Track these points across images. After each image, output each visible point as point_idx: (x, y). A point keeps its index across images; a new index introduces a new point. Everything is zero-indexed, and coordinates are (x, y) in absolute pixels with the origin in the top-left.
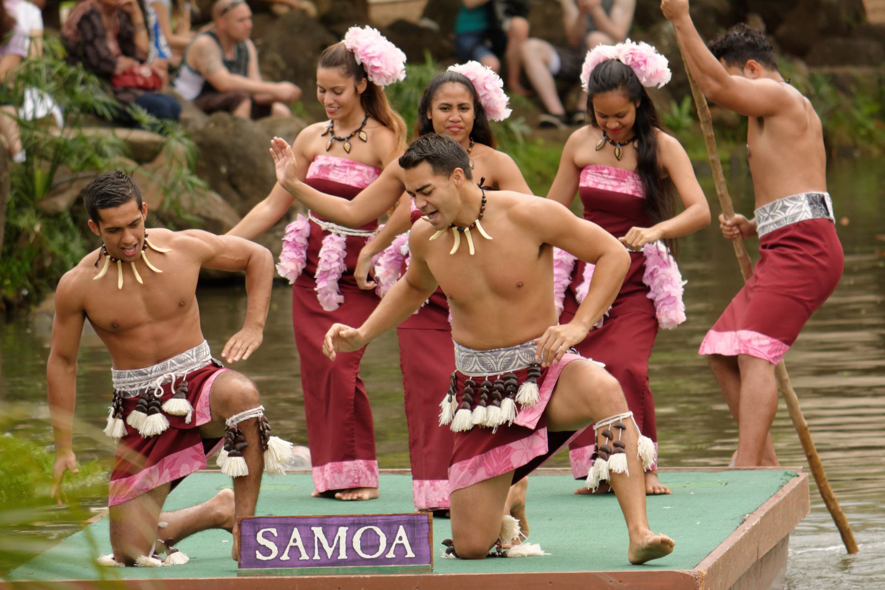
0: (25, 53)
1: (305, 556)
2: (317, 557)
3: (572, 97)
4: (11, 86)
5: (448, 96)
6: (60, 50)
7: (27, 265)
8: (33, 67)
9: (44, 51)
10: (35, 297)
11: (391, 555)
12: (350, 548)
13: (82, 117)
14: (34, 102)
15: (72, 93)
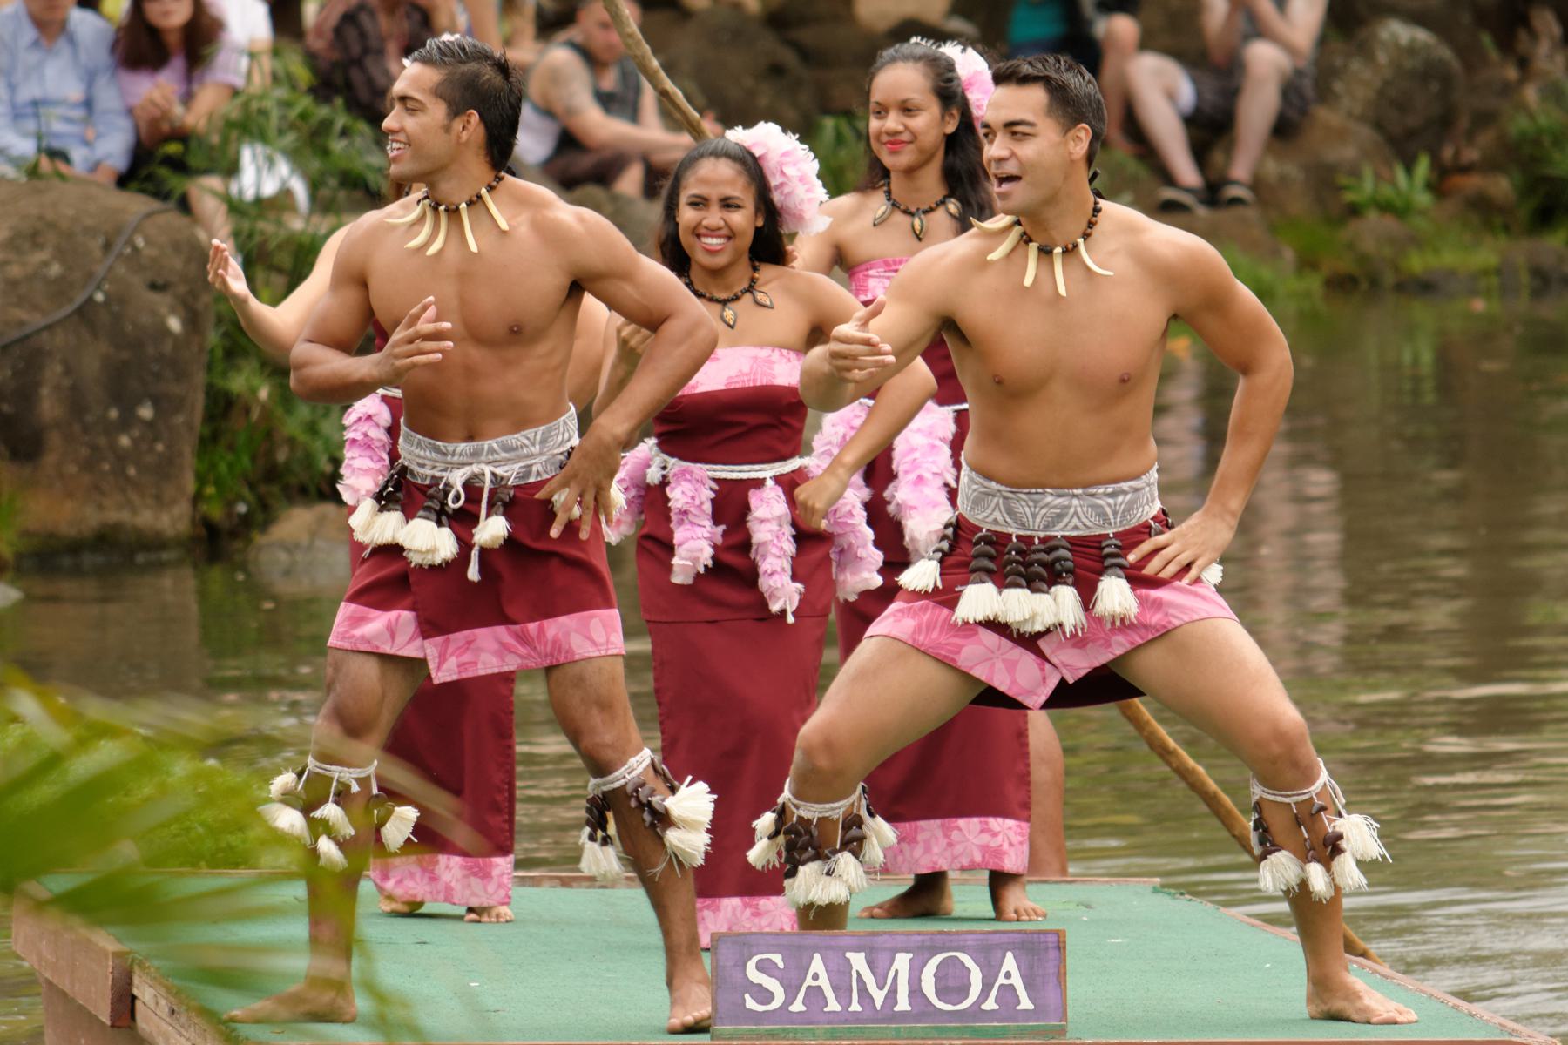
0: (239, 82)
1: (833, 1005)
2: (855, 1007)
3: (1217, 157)
4: (215, 139)
5: (704, 181)
6: (303, 75)
7: (246, 461)
8: (255, 105)
9: (275, 78)
10: (260, 517)
11: (990, 1005)
12: (916, 992)
13: (342, 195)
14: (259, 171)
15: (325, 152)
